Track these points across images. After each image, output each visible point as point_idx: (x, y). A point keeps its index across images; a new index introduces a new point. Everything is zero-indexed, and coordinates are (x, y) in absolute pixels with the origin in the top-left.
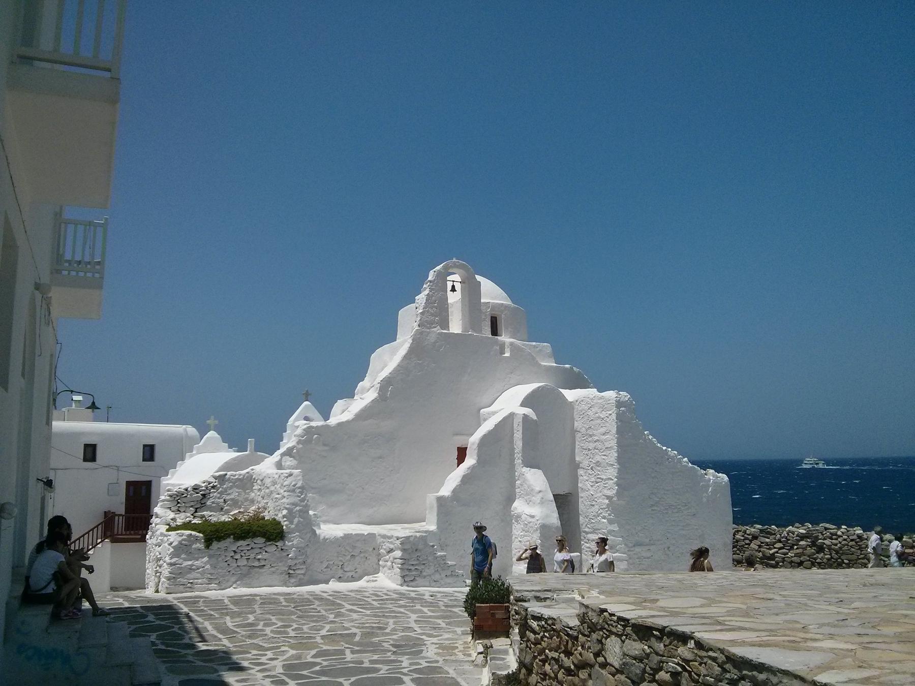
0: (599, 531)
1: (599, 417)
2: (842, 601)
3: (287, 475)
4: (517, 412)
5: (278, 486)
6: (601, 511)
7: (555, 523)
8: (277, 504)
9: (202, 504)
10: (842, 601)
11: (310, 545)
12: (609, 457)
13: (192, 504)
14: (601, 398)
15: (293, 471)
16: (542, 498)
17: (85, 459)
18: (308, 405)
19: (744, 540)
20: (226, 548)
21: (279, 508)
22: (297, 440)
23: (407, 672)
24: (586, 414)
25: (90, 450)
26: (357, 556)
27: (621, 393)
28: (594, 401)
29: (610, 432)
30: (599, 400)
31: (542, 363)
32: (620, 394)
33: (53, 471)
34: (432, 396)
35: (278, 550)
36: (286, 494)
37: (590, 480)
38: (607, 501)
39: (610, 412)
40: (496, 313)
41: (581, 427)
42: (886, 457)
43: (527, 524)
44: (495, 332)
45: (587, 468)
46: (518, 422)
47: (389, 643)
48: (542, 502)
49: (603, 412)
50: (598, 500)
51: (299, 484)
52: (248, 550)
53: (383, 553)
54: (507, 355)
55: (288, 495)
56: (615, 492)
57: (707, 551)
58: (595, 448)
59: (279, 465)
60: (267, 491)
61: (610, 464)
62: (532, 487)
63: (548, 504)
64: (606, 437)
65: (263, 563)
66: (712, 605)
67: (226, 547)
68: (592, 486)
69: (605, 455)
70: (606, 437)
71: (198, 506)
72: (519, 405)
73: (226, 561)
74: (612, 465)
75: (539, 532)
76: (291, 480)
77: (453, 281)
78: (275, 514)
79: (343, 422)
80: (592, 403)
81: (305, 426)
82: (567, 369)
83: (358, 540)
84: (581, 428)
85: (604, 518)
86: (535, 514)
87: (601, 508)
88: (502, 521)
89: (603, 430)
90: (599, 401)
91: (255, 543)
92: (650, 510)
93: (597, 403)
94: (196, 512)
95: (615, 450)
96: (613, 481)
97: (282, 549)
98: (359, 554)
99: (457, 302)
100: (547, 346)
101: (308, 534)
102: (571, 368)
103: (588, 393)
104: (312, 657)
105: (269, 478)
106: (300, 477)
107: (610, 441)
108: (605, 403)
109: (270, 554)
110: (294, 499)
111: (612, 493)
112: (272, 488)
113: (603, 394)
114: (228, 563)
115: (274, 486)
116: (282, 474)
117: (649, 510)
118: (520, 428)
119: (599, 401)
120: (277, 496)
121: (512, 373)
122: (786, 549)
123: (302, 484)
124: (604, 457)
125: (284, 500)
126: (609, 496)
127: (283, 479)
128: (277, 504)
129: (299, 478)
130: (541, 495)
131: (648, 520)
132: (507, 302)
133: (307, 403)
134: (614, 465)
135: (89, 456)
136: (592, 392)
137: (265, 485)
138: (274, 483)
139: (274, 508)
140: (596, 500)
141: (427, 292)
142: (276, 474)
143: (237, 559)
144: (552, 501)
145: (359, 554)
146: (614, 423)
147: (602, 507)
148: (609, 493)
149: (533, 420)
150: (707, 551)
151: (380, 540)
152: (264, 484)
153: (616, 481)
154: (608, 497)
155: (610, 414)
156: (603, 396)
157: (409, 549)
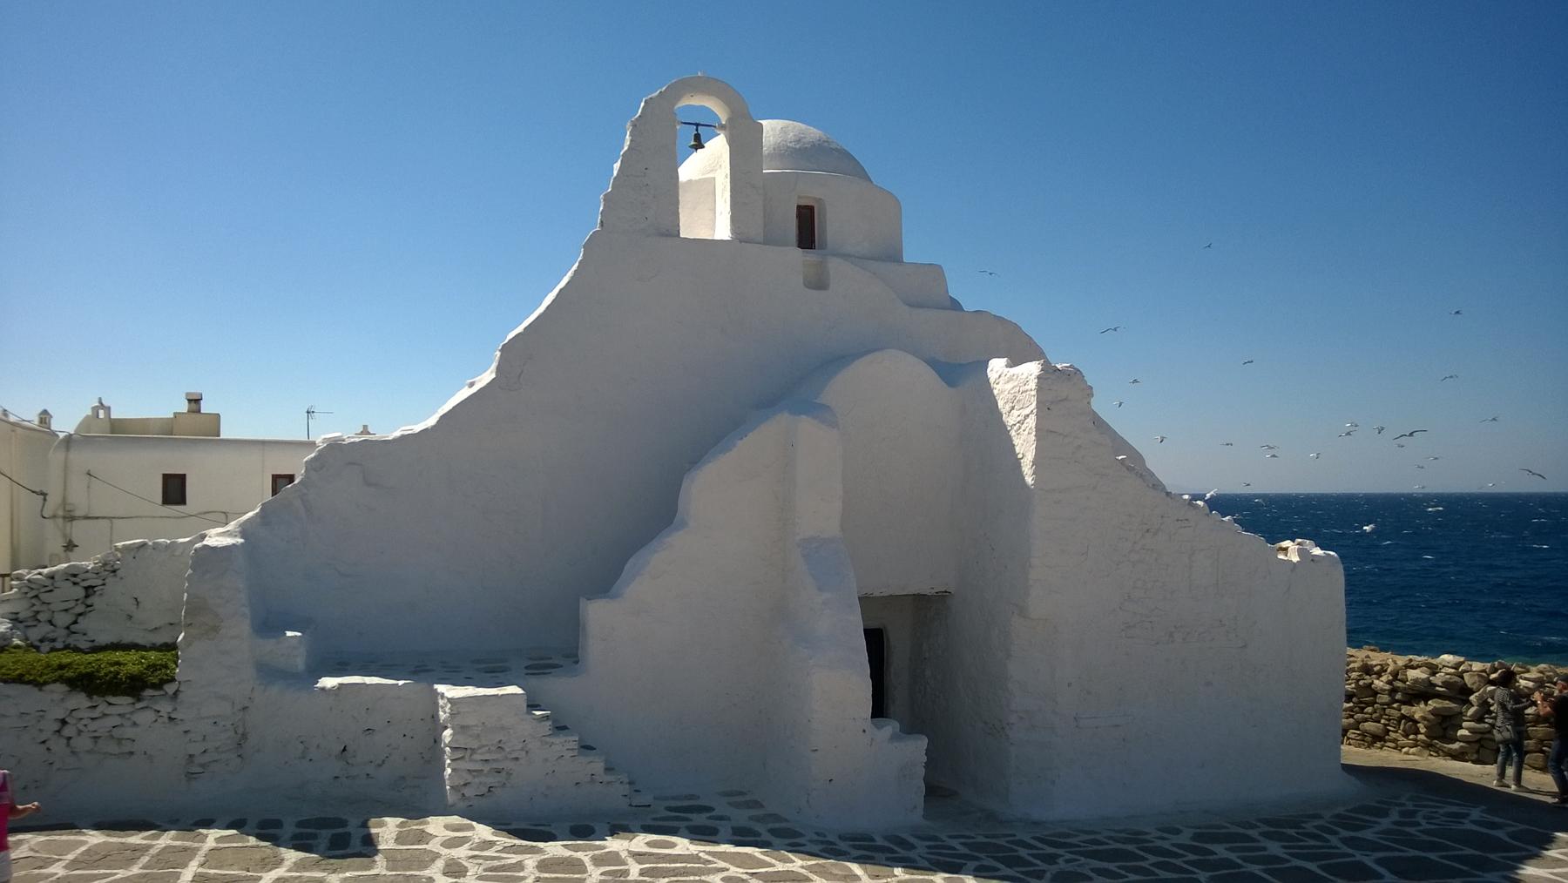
9: (88, 606)
13: (66, 605)
17: (182, 478)
19: (1358, 722)
20: (41, 713)
35: (159, 720)
42: (1532, 861)
47: (1184, 859)
52: (92, 719)
57: (45, 412)
65: (127, 747)
71: (80, 609)
73: (44, 742)
77: (697, 125)
94: (75, 622)
97: (171, 719)
104: (794, 862)
114: (48, 744)
122: (1411, 619)
129: (1015, 413)
150: (45, 412)
157: (476, 726)
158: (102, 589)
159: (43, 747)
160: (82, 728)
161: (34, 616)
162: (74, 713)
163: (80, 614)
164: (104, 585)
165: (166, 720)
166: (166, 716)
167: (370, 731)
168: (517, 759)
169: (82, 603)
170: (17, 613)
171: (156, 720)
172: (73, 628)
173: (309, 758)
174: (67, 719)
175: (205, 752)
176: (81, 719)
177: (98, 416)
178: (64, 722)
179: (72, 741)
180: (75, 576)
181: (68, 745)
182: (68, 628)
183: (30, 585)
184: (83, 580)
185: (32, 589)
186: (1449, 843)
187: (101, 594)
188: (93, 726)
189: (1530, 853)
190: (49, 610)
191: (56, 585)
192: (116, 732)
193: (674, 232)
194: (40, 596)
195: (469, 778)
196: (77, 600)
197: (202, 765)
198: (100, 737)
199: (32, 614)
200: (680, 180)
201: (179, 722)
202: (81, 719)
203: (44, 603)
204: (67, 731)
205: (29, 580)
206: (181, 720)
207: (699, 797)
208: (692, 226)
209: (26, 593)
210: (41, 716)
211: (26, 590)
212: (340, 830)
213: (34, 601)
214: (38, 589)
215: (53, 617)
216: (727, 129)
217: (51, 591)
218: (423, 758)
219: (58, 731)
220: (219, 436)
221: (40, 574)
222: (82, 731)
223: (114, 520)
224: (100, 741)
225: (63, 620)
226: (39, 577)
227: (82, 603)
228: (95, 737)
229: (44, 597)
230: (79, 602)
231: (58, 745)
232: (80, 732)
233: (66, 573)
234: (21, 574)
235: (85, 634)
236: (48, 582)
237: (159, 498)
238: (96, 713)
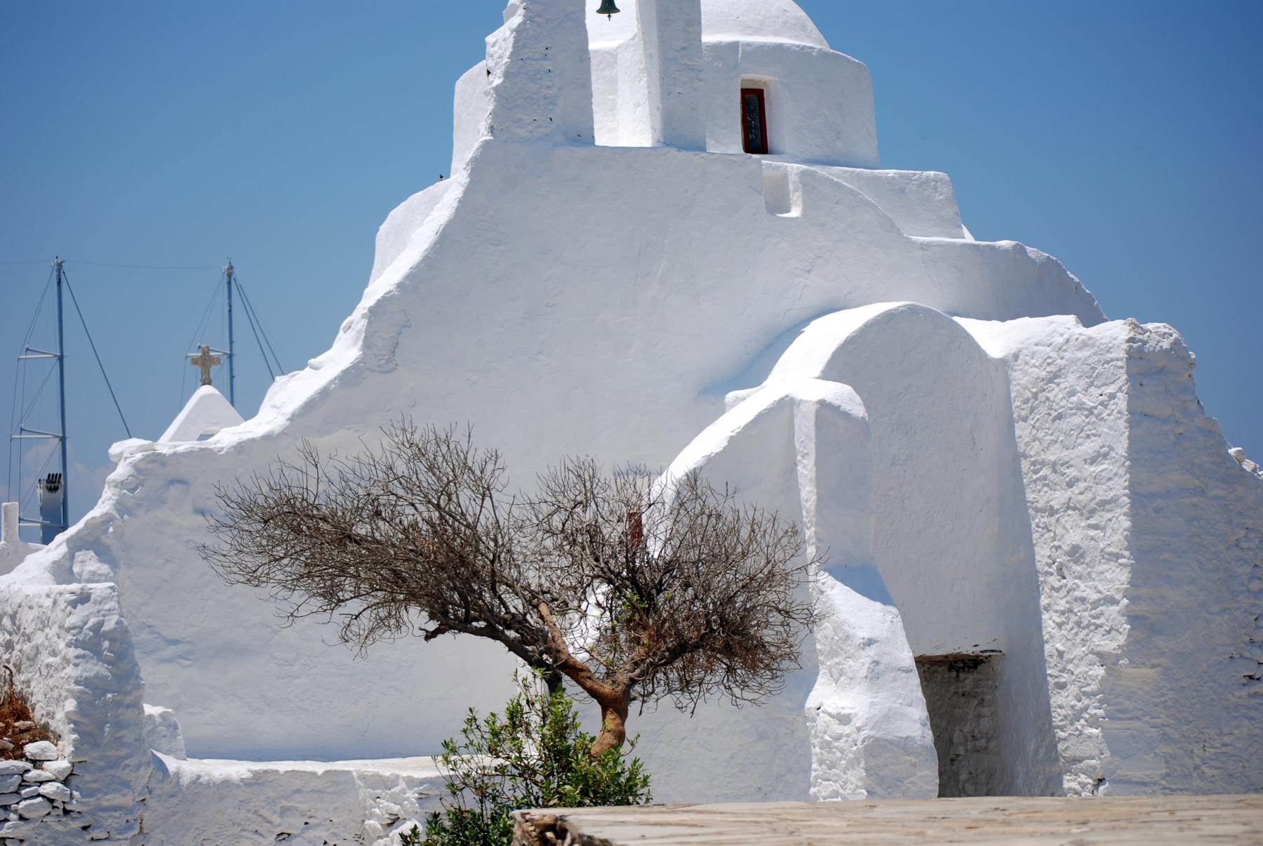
0: (1079, 766)
1: (1080, 407)
2: (640, 714)
3: (73, 598)
4: (799, 395)
5: (52, 631)
6: (1086, 701)
7: (912, 738)
8: (51, 682)
10: (640, 714)
11: (150, 802)
12: (1109, 531)
14: (1084, 345)
15: (90, 585)
16: (877, 663)
18: (211, 395)
21: (55, 693)
22: (115, 498)
24: (1042, 397)
26: (298, 836)
27: (1150, 326)
28: (1068, 355)
29: (1113, 454)
30: (1080, 349)
31: (914, 238)
32: (1146, 331)
34: (540, 353)
35: (54, 812)
36: (72, 652)
37: (1056, 608)
38: (1100, 671)
39: (1111, 389)
41: (1027, 439)
43: (828, 743)
44: (756, 140)
45: (1046, 569)
46: (805, 428)
48: (876, 675)
49: (1092, 389)
50: (1077, 666)
51: (109, 625)
53: (375, 829)
54: (795, 212)
55: (77, 657)
56: (1122, 639)
58: (1068, 508)
59: (62, 572)
60: (27, 647)
61: (1110, 554)
62: (846, 628)
63: (895, 680)
68: (1060, 625)
69: (1095, 527)
72: (818, 374)
74: (1117, 556)
75: (863, 764)
76: (86, 613)
78: (48, 714)
79: (253, 440)
80: (1063, 362)
81: (139, 456)
82: (1005, 251)
83: (298, 791)
84: (1027, 444)
85: (1093, 722)
86: (852, 711)
87: (1085, 694)
88: (762, 736)
89: (1089, 447)
92: (1244, 692)
93: (1073, 362)
95: (1125, 510)
96: (1117, 608)
98: (303, 830)
99: (624, 47)
100: (936, 180)
101: (142, 771)
102: (1019, 250)
105: (31, 608)
106: (112, 604)
107: (1110, 479)
108: (1096, 358)
109: (32, 825)
110: (97, 668)
111: (1114, 645)
112: (39, 638)
113: (1094, 331)
115: (42, 630)
116: (61, 594)
117: (1237, 693)
118: (811, 447)
120: (51, 660)
121: (809, 271)
123: (117, 623)
124: (1092, 533)
125: (70, 670)
126: (1109, 654)
127: (63, 611)
128: (51, 682)
130: (871, 652)
131: (1237, 727)
132: (810, 39)
133: (206, 390)
134: (1123, 557)
136: (1066, 324)
137: (22, 630)
138: (44, 624)
139: (45, 695)
140: (1070, 667)
141: (516, 20)
142: (48, 596)
144: (907, 671)
145: (303, 830)
146: (1122, 424)
147: (1088, 689)
148: (1109, 645)
151: (364, 792)
152: (19, 629)
153: (1127, 606)
154: (1103, 658)
155: (1112, 396)
156: (1090, 338)
165: (60, 812)
193: (583, 137)
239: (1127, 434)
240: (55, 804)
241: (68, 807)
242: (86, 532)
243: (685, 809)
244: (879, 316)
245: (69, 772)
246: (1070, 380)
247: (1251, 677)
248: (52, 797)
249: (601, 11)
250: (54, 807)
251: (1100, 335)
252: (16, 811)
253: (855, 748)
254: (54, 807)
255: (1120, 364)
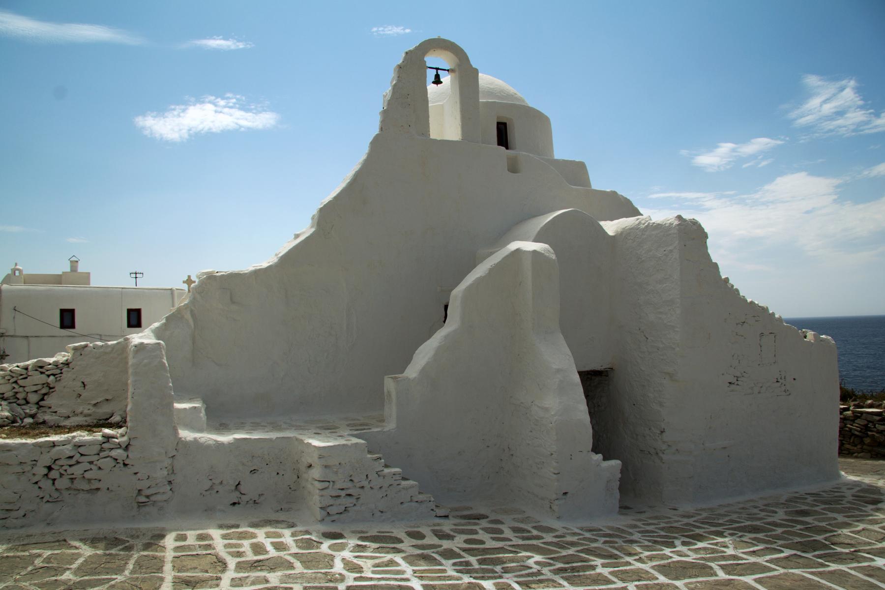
13: (35, 388)
20: (34, 462)
23: (577, 541)
25: (134, 315)
33: (25, 341)
35: (118, 466)
39: (670, 248)
40: (505, 116)
46: (527, 265)
52: (70, 466)
64: (665, 285)
65: (95, 485)
66: (859, 415)
67: (35, 460)
70: (665, 285)
73: (36, 483)
77: (437, 69)
90: (653, 233)
91: (82, 455)
94: (42, 399)
103: (637, 222)
114: (40, 484)
119: (653, 233)
135: (134, 322)
143: (54, 480)
149: (144, 114)
155: (671, 251)
158: (61, 376)
159: (36, 486)
160: (63, 472)
161: (14, 395)
162: (56, 462)
163: (45, 394)
164: (61, 373)
165: (122, 465)
166: (122, 462)
167: (255, 471)
168: (363, 487)
169: (47, 386)
170: (3, 394)
171: (115, 466)
172: (41, 403)
173: (216, 490)
174: (53, 466)
175: (149, 487)
176: (62, 466)
177: (15, 274)
178: (50, 468)
179: (56, 482)
180: (41, 367)
181: (54, 484)
182: (37, 403)
183: (11, 374)
184: (48, 371)
185: (13, 377)
186: (686, 527)
187: (60, 380)
188: (70, 470)
189: (659, 534)
190: (25, 391)
191: (30, 373)
192: (87, 475)
194: (18, 381)
195: (331, 502)
196: (43, 384)
197: (148, 497)
198: (76, 478)
199: (13, 394)
200: (480, 83)
201: (131, 467)
202: (62, 466)
203: (21, 386)
204: (54, 474)
205: (11, 371)
206: (132, 465)
207: (471, 508)
208: (435, 133)
209: (9, 380)
210: (34, 465)
211: (9, 377)
212: (295, 538)
213: (14, 385)
214: (17, 377)
215: (27, 396)
216: (457, 73)
217: (26, 378)
218: (290, 488)
219: (46, 475)
220: (89, 285)
221: (18, 366)
222: (63, 475)
223: (30, 339)
224: (75, 482)
225: (33, 398)
226: (17, 368)
227: (47, 386)
228: (72, 479)
229: (21, 382)
230: (45, 386)
231: (46, 484)
232: (61, 475)
233: (36, 366)
234: (5, 367)
235: (50, 408)
236: (24, 372)
237: (58, 324)
238: (72, 462)
239: (679, 269)
240: (118, 461)
241: (126, 462)
242: (177, 312)
243: (396, 576)
244: (550, 121)
245: (128, 443)
246: (131, 565)
247: (730, 383)
248: (116, 458)
249: (434, 83)
250: (118, 463)
251: (664, 223)
252: (96, 465)
253: (551, 425)
254: (118, 463)
255: (675, 236)
